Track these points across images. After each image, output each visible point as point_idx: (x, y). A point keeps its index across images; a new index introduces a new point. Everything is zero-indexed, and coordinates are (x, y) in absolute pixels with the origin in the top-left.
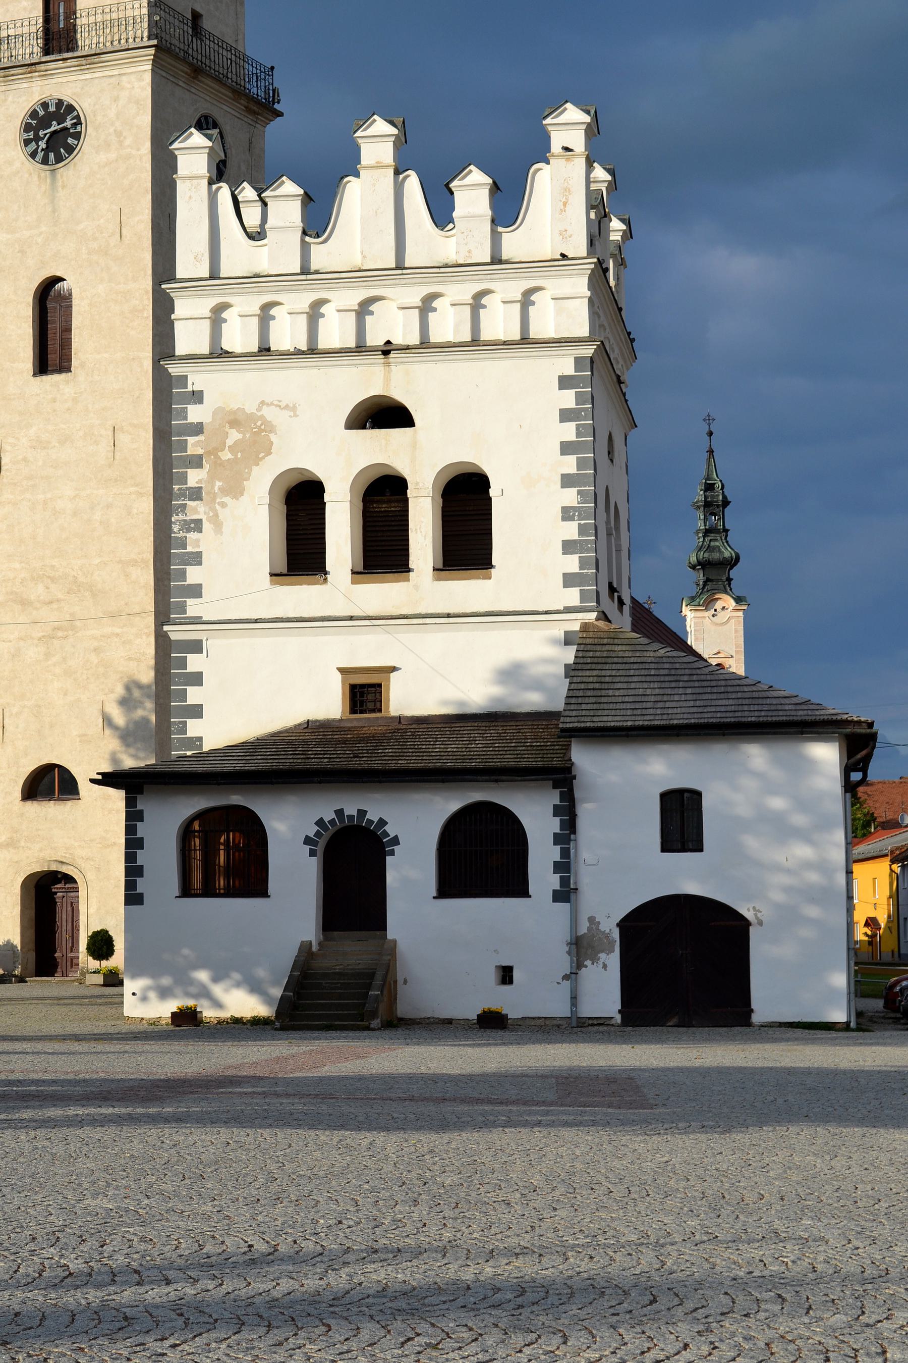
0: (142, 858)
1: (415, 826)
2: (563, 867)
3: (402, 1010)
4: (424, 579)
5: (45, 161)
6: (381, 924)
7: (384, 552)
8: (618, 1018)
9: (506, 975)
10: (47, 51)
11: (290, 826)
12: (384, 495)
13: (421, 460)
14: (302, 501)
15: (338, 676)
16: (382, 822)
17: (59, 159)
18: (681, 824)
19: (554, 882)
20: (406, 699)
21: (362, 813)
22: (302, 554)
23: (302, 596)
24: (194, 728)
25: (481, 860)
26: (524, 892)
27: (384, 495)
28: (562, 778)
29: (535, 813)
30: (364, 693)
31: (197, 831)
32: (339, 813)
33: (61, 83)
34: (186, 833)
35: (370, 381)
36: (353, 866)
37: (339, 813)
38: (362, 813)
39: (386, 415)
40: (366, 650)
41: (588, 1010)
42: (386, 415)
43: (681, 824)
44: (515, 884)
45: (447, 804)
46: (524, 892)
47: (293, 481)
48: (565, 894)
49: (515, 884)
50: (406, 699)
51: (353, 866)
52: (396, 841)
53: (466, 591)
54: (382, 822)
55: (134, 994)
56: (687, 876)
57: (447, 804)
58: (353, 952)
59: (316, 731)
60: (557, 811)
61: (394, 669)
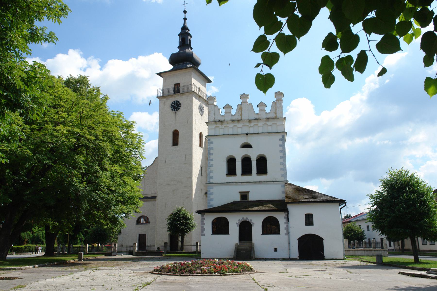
0: (205, 227)
1: (257, 221)
2: (287, 228)
3: (256, 256)
4: (254, 176)
5: (174, 111)
6: (251, 240)
7: (247, 171)
8: (298, 258)
9: (276, 250)
10: (175, 93)
11: (234, 221)
12: (246, 161)
13: (253, 154)
14: (231, 162)
15: (239, 193)
16: (251, 220)
17: (177, 110)
18: (309, 220)
19: (285, 231)
20: (251, 198)
21: (247, 218)
22: (231, 171)
23: (232, 179)
24: (212, 203)
25: (271, 227)
26: (279, 233)
27: (246, 161)
28: (286, 210)
29: (280, 217)
30: (244, 196)
31: (98, 245)
32: (243, 218)
33: (177, 98)
34: (213, 223)
35: (244, 140)
36: (245, 229)
37: (243, 218)
38: (247, 218)
39: (247, 146)
40: (244, 188)
41: (292, 257)
42: (247, 146)
43: (309, 220)
44: (277, 232)
45: (265, 215)
46: (279, 233)
47: (232, 157)
48: (288, 233)
49: (277, 232)
50: (251, 198)
51: (245, 229)
52: (254, 224)
53: (262, 178)
54: (251, 220)
55: (276, 250)
56: (310, 230)
57: (265, 215)
58: (246, 245)
59: (234, 203)
60: (285, 218)
61: (249, 192)
